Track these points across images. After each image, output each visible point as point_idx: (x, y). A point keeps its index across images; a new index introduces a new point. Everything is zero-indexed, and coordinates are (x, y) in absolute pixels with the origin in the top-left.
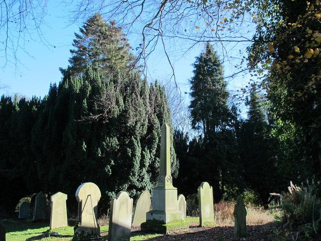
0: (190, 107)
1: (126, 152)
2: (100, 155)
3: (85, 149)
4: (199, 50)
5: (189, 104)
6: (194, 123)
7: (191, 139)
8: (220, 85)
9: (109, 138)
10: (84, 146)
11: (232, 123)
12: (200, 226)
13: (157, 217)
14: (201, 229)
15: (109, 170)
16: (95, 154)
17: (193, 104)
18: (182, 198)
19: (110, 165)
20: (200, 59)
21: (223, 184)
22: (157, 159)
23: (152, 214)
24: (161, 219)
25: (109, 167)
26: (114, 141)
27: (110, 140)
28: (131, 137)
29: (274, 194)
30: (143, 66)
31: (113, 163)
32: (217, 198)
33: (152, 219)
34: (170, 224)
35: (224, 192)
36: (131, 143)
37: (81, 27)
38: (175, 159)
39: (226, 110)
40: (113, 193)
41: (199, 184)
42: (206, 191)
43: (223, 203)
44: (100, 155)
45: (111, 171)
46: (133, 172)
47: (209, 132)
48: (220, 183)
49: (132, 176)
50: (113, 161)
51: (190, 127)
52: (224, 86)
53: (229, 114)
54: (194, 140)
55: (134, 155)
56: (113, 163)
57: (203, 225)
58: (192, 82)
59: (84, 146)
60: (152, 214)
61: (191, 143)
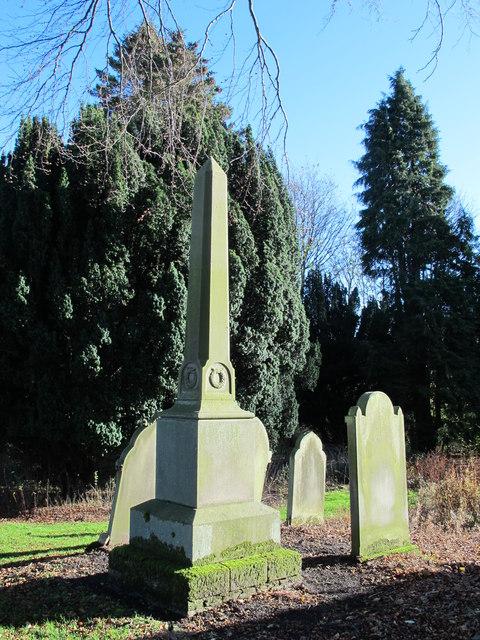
0: (359, 226)
1: (150, 306)
2: (68, 316)
3: (26, 296)
4: (380, 92)
5: (358, 219)
6: (367, 261)
7: (363, 304)
8: (428, 171)
9: (101, 268)
10: (24, 286)
11: (458, 261)
12: (352, 560)
13: (161, 529)
14: (351, 582)
15: (92, 361)
16: (55, 309)
17: (368, 218)
18: (311, 444)
19: (97, 344)
20: (378, 114)
21: (438, 406)
22: (249, 330)
23: (147, 518)
24: (176, 543)
25: (95, 350)
26: (117, 274)
27: (103, 274)
28: (168, 266)
29: (96, 477)
30: (464, 526)
31: (106, 337)
32: (420, 441)
33: (147, 537)
34: (206, 570)
35: (441, 423)
36: (168, 279)
37: (111, 55)
38: (307, 334)
39: (441, 224)
40: (113, 426)
41: (354, 399)
42: (121, 197)
43: (436, 461)
44: (68, 316)
45: (98, 362)
46: (170, 364)
47: (405, 280)
48: (431, 401)
49: (167, 378)
50: (106, 333)
51: (359, 270)
52: (439, 173)
53: (454, 240)
54: (372, 304)
55: (172, 315)
56: (106, 337)
57: (364, 555)
58: (361, 166)
59: (24, 286)
60: (147, 518)
61: (365, 311)
